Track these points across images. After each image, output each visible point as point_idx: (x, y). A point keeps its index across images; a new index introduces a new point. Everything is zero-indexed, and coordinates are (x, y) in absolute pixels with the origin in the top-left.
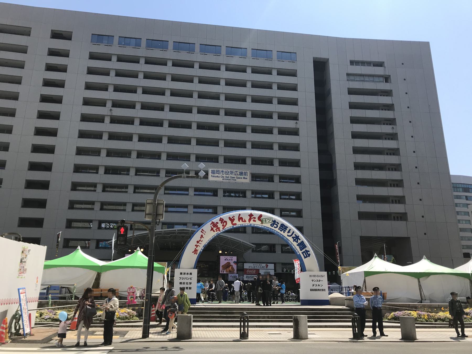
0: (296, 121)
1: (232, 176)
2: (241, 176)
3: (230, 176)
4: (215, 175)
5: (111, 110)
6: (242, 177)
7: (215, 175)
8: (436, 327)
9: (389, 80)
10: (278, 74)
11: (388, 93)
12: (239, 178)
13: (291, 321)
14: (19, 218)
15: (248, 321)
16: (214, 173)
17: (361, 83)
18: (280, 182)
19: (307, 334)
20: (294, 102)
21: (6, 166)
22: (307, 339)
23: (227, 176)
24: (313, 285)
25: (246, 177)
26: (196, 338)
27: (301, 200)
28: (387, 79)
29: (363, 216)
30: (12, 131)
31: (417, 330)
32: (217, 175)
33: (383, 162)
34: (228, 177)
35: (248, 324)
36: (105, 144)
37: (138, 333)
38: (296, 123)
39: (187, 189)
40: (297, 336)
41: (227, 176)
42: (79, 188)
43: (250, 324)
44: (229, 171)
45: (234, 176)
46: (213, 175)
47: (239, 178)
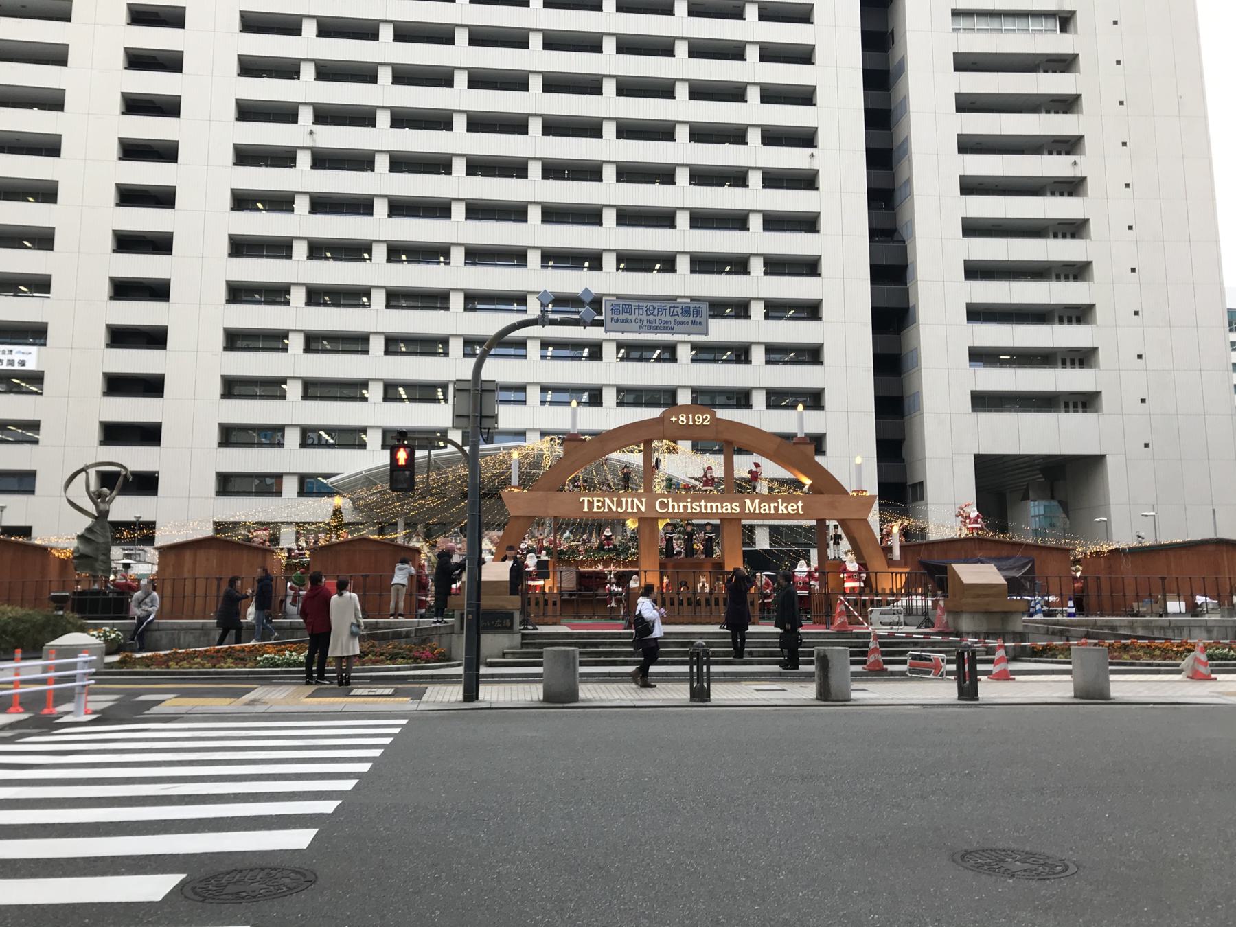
0: (809, 150)
1: (664, 318)
2: (686, 319)
3: (657, 318)
4: (620, 317)
5: (311, 133)
7: (620, 317)
8: (1158, 672)
9: (1071, 27)
10: (761, 18)
11: (1064, 63)
12: (682, 323)
15: (709, 663)
16: (618, 313)
19: (848, 691)
23: (652, 318)
24: (11, 351)
25: (698, 319)
26: (589, 700)
27: (821, 363)
28: (1065, 21)
29: (983, 401)
30: (56, 195)
31: (1112, 677)
32: (626, 316)
35: (708, 669)
37: (455, 693)
38: (812, 155)
40: (825, 694)
41: (652, 318)
43: (713, 669)
45: (668, 318)
46: (616, 317)
47: (682, 323)
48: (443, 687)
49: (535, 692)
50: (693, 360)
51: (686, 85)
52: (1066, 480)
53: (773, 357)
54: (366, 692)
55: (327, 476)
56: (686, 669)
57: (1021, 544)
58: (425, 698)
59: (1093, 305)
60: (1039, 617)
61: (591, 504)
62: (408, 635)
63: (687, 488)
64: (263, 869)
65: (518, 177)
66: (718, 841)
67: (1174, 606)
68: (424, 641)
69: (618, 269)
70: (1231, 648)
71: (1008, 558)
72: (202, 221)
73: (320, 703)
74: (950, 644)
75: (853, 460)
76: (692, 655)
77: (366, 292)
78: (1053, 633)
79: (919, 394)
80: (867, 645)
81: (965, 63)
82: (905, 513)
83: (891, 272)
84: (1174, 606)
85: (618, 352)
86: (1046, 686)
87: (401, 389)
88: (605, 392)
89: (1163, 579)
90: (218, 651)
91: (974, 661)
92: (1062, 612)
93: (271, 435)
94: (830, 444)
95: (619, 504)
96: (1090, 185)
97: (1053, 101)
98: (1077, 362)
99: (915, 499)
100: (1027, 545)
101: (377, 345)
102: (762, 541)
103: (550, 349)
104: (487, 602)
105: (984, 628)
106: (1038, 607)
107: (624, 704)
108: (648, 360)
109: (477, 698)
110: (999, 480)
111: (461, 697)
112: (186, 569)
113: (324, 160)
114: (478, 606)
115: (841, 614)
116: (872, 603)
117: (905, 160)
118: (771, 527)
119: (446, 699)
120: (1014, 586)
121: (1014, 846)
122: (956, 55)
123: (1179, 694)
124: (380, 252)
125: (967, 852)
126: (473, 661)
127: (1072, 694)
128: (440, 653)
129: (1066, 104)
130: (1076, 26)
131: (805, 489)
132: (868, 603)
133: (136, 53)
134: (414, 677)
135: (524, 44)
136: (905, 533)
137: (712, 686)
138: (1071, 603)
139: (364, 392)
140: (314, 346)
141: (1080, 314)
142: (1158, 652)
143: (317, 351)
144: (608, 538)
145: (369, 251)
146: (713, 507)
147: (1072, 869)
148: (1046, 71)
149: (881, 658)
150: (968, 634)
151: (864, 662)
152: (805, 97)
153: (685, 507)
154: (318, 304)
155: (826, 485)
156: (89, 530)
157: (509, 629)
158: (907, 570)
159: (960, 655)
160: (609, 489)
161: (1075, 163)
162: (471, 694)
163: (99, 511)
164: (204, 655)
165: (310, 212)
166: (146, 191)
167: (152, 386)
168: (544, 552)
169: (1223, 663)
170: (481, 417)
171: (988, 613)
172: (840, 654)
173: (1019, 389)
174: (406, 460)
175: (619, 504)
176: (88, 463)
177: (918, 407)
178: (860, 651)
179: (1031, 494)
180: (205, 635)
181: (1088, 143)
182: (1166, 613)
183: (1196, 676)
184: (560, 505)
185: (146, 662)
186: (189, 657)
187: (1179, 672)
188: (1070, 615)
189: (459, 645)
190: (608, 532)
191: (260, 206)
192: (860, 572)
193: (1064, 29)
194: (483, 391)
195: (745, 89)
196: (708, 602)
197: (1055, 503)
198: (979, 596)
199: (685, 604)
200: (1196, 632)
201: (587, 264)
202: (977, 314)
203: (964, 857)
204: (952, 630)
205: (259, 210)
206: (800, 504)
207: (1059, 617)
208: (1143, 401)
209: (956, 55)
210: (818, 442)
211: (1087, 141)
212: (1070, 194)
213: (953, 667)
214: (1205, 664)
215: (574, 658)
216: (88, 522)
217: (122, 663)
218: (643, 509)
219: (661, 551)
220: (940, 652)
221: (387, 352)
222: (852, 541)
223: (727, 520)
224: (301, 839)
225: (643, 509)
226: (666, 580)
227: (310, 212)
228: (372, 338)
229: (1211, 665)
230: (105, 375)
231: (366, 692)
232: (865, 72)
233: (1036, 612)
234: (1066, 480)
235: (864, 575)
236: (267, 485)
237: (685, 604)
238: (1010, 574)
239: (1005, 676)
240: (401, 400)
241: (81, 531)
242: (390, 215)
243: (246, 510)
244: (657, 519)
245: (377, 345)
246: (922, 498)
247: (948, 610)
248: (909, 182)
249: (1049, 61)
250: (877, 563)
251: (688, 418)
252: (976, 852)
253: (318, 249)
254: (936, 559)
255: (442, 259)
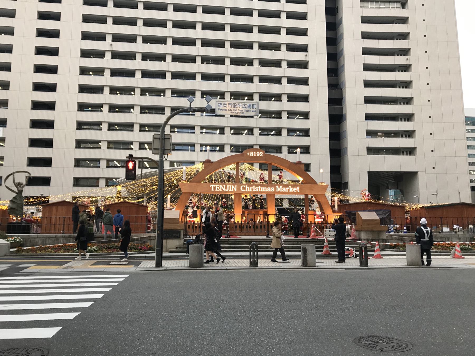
1: (240, 109)
4: (222, 108)
5: (111, 45)
6: (251, 110)
7: (222, 108)
8: (440, 255)
9: (406, 7)
12: (248, 111)
13: (300, 251)
14: (28, 158)
15: (258, 251)
16: (221, 106)
17: (376, 9)
18: (288, 135)
20: (304, 32)
21: (7, 123)
22: (316, 266)
23: (235, 109)
27: (309, 136)
29: (372, 151)
30: (10, 68)
33: (395, 112)
34: (236, 110)
35: (257, 253)
36: (106, 98)
37: (151, 264)
38: (306, 55)
39: (193, 128)
40: (305, 264)
42: (85, 127)
43: (259, 253)
44: (237, 103)
45: (242, 109)
46: (220, 108)
47: (248, 111)
48: (149, 261)
49: (184, 264)
50: (260, 134)
51: (257, 28)
52: (404, 181)
53: (291, 134)
54: (116, 263)
55: (116, 179)
56: (248, 253)
57: (385, 205)
58: (140, 266)
59: (414, 114)
60: (392, 233)
61: (215, 188)
62: (137, 240)
63: (253, 181)
64: (25, 348)
65: (192, 63)
66: (247, 332)
67: (445, 229)
68: (144, 243)
69: (231, 99)
70: (469, 246)
71: (381, 210)
72: (68, 79)
73: (95, 268)
74: (357, 244)
75: (321, 172)
76: (251, 248)
77: (132, 107)
78: (398, 240)
79: (346, 148)
80: (323, 244)
81: (365, 20)
82: (340, 193)
83: (336, 100)
84: (445, 229)
85: (231, 131)
86: (396, 261)
87: (146, 145)
88: (225, 146)
89: (441, 218)
90: (59, 246)
91: (366, 251)
92: (401, 231)
93: (95, 163)
94: (312, 167)
95: (226, 188)
96: (413, 68)
97: (399, 35)
98: (407, 136)
99: (345, 189)
100: (388, 205)
101: (136, 128)
102: (286, 205)
103: (204, 130)
104: (166, 227)
105: (370, 238)
106: (392, 229)
107: (222, 268)
108: (242, 134)
109: (161, 266)
110: (378, 182)
111: (154, 266)
112: (53, 214)
113: (116, 55)
114: (162, 227)
115: (313, 231)
116: (326, 227)
117: (342, 57)
118: (290, 199)
119: (149, 266)
120: (383, 221)
121: (382, 334)
122: (363, 49)
123: (449, 264)
124: (138, 92)
125: (361, 338)
126: (160, 252)
127: (406, 264)
128: (150, 247)
129: (404, 36)
130: (408, 6)
131: (300, 182)
132: (325, 227)
133: (42, 13)
134: (138, 257)
135: (195, 11)
136: (341, 201)
137: (259, 261)
138: (405, 228)
139: (132, 146)
140: (112, 128)
141: (409, 117)
142: (440, 247)
143: (113, 130)
144: (225, 202)
145: (134, 91)
146: (263, 189)
147: (410, 347)
148: (396, 24)
149: (329, 249)
150: (364, 240)
151: (322, 251)
152: (304, 32)
153: (252, 189)
154: (114, 112)
155: (309, 181)
156: (14, 198)
157: (179, 237)
158: (341, 214)
159: (361, 248)
160: (223, 182)
161: (407, 59)
162: (159, 264)
163: (18, 191)
164: (53, 248)
165: (111, 76)
166: (46, 67)
167: (48, 143)
168: (195, 207)
169: (466, 251)
170: (164, 149)
171: (372, 231)
172: (311, 247)
173: (384, 129)
174: (133, 167)
175: (226, 188)
176: (14, 171)
177: (346, 136)
178: (320, 247)
179: (389, 187)
180: (57, 240)
181: (412, 52)
182: (442, 232)
183: (455, 257)
184: (202, 188)
185: (28, 251)
186: (45, 249)
187: (449, 255)
188: (405, 232)
189: (154, 243)
190: (224, 200)
191: (91, 73)
192: (321, 215)
193: (403, 7)
194: (165, 138)
195: (280, 29)
196: (261, 227)
197: (398, 190)
198: (368, 224)
199: (252, 228)
200: (454, 239)
201: (219, 97)
202: (369, 117)
203: (359, 340)
204: (358, 238)
205: (117, 94)
206: (298, 188)
207: (400, 233)
208: (432, 151)
209: (363, 49)
210: (307, 167)
211: (412, 50)
212: (405, 71)
213: (358, 253)
214: (460, 252)
215: (202, 249)
216: (14, 195)
217: (17, 251)
218: (236, 190)
219: (243, 207)
220: (353, 247)
221: (140, 131)
222: (319, 203)
223: (269, 194)
224: (49, 333)
225: (236, 190)
226: (244, 218)
227: (111, 76)
228: (135, 125)
229: (462, 252)
230: (29, 139)
231: (116, 263)
232: (327, 23)
233: (391, 231)
234: (404, 181)
235: (323, 217)
236: (94, 182)
237: (252, 228)
238: (381, 216)
239: (379, 257)
240: (146, 149)
241: (11, 198)
242: (142, 77)
243: (84, 192)
244: (241, 194)
245: (136, 128)
246: (348, 188)
247: (356, 230)
248: (343, 66)
249: (397, 19)
250: (329, 211)
251: (254, 154)
252: (365, 338)
253: (113, 90)
254: (352, 210)
255: (162, 94)
